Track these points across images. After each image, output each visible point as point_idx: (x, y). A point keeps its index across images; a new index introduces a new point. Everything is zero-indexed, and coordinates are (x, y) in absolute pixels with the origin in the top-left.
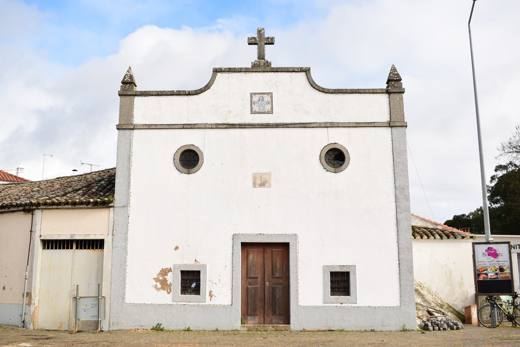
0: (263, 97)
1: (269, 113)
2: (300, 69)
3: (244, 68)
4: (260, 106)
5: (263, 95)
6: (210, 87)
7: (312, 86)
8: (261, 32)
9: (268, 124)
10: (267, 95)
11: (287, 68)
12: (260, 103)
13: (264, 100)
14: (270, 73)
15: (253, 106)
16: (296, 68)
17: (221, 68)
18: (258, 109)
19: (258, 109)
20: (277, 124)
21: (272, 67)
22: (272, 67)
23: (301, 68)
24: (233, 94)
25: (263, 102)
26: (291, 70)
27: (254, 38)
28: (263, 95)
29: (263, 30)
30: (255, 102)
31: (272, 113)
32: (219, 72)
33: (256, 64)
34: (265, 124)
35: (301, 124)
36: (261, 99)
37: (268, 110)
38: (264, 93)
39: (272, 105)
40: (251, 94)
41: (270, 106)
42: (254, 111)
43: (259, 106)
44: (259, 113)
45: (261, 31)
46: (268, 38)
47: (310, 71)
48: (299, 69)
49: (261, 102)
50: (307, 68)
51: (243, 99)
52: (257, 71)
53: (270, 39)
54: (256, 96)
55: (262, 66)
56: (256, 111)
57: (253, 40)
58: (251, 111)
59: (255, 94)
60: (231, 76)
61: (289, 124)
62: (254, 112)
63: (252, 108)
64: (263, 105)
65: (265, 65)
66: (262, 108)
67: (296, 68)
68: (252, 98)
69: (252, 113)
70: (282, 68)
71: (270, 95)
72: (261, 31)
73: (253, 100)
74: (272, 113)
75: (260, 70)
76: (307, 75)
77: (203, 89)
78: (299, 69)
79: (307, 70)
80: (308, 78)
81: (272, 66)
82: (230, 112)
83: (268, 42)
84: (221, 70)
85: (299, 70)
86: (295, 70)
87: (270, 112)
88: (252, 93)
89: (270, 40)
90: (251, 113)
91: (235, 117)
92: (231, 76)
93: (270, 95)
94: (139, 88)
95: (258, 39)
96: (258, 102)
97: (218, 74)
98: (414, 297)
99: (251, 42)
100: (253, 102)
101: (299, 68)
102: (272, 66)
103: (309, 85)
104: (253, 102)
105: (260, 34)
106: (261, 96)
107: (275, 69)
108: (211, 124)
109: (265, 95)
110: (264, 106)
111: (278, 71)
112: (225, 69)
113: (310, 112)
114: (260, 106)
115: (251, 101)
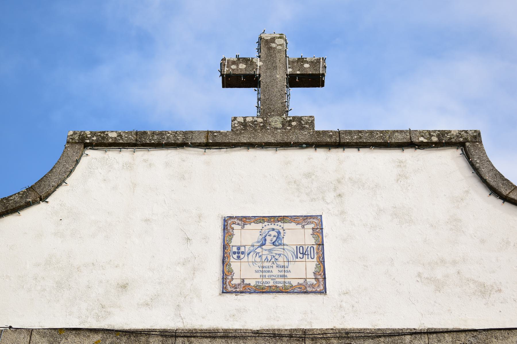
0: (279, 233)
1: (309, 289)
2: (438, 136)
3: (200, 132)
4: (266, 264)
5: (280, 223)
6: (48, 195)
7: (494, 191)
8: (273, 45)
9: (305, 331)
10: (299, 226)
11: (381, 132)
12: (265, 252)
13: (285, 241)
14: (310, 153)
15: (235, 265)
16: (421, 133)
17: (104, 132)
18: (258, 275)
19: (258, 275)
20: (347, 333)
21: (316, 129)
22: (316, 129)
23: (442, 134)
24: (147, 220)
25: (278, 250)
26: (399, 138)
27: (247, 61)
28: (278, 226)
29: (280, 38)
30: (242, 249)
31: (320, 293)
32: (92, 146)
33: (253, 122)
34: (291, 330)
35: (464, 334)
36: (268, 238)
37: (301, 281)
38: (283, 219)
39: (322, 262)
40: (225, 221)
41: (311, 265)
42: (235, 282)
43: (260, 264)
44: (261, 290)
45: (274, 42)
46: (301, 60)
47: (481, 142)
48: (431, 136)
49: (270, 250)
50: (466, 132)
51: (188, 239)
52: (253, 140)
53: (307, 62)
54: (247, 227)
55: (276, 129)
56: (246, 282)
57: (242, 66)
58: (224, 283)
59: (244, 220)
60: (145, 161)
61: (405, 334)
62: (235, 286)
63: (231, 272)
64: (281, 259)
65: (290, 125)
66: (275, 271)
67: (420, 132)
68: (233, 235)
69: (229, 289)
70: (360, 132)
71: (312, 226)
72: (274, 42)
73: (236, 241)
74: (324, 292)
75: (266, 140)
76: (467, 155)
77: (17, 199)
78: (431, 136)
79: (466, 140)
80: (472, 165)
81: (318, 127)
82: (124, 287)
83: (298, 72)
84: (103, 138)
85: (435, 139)
86: (415, 140)
87: (312, 285)
88: (231, 218)
89: (306, 66)
90: (225, 291)
91: (147, 304)
92: (145, 161)
93: (312, 226)
94: (251, 285)
95: (259, 64)
96: (259, 250)
97: (88, 152)
98: (117, 143)
99: (233, 70)
100: (235, 249)
101: (435, 131)
102: (318, 127)
103: (484, 192)
104: (235, 249)
105: (270, 48)
106: (272, 226)
107: (331, 136)
108: (27, 330)
109: (286, 226)
110: (282, 264)
111: (342, 141)
112: (120, 135)
113: (500, 291)
114: (266, 264)
115: (225, 247)
